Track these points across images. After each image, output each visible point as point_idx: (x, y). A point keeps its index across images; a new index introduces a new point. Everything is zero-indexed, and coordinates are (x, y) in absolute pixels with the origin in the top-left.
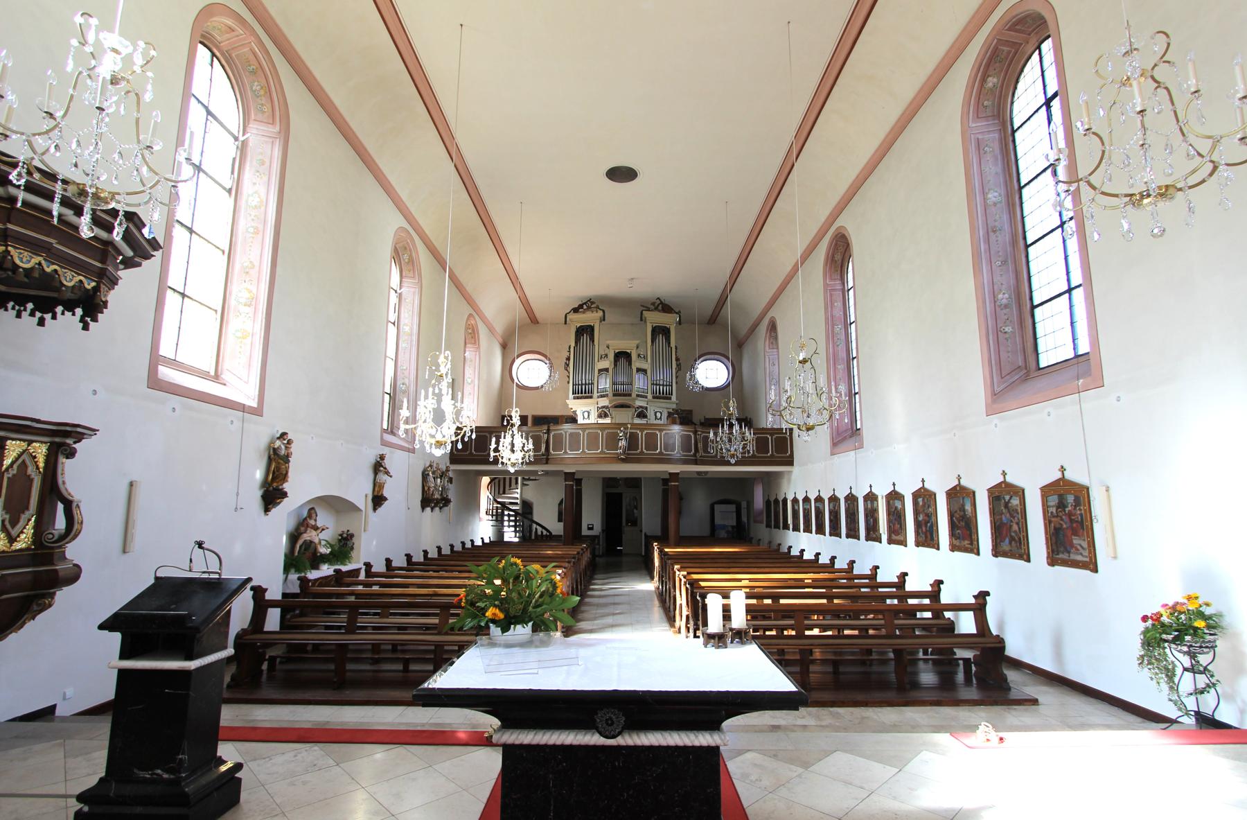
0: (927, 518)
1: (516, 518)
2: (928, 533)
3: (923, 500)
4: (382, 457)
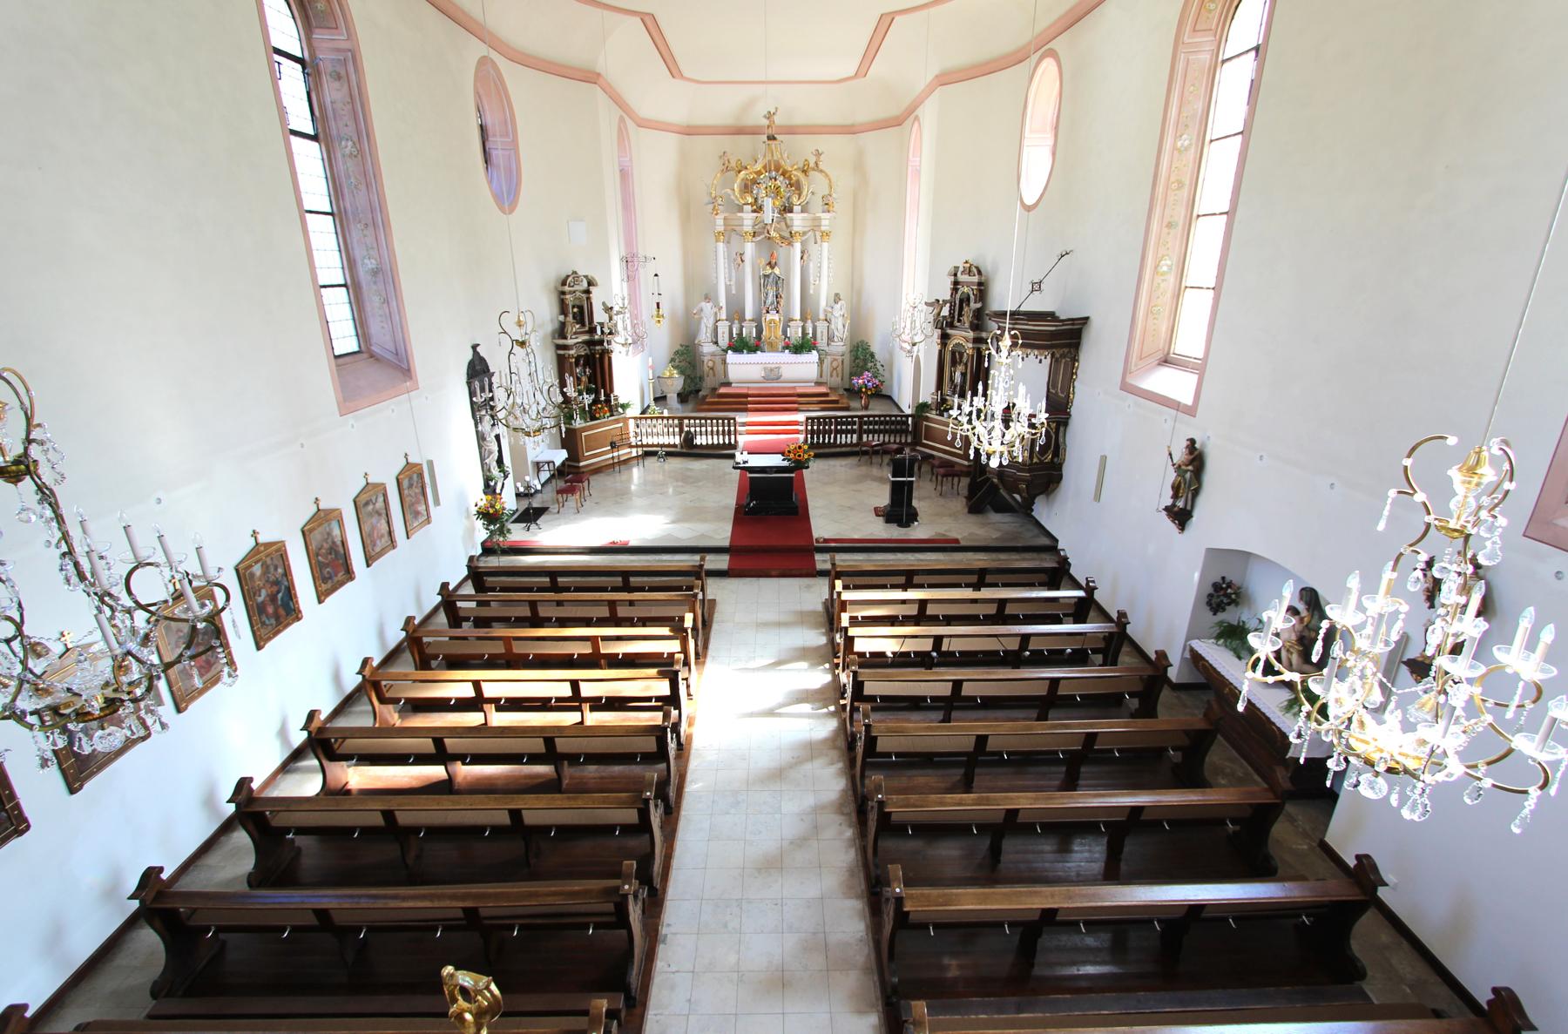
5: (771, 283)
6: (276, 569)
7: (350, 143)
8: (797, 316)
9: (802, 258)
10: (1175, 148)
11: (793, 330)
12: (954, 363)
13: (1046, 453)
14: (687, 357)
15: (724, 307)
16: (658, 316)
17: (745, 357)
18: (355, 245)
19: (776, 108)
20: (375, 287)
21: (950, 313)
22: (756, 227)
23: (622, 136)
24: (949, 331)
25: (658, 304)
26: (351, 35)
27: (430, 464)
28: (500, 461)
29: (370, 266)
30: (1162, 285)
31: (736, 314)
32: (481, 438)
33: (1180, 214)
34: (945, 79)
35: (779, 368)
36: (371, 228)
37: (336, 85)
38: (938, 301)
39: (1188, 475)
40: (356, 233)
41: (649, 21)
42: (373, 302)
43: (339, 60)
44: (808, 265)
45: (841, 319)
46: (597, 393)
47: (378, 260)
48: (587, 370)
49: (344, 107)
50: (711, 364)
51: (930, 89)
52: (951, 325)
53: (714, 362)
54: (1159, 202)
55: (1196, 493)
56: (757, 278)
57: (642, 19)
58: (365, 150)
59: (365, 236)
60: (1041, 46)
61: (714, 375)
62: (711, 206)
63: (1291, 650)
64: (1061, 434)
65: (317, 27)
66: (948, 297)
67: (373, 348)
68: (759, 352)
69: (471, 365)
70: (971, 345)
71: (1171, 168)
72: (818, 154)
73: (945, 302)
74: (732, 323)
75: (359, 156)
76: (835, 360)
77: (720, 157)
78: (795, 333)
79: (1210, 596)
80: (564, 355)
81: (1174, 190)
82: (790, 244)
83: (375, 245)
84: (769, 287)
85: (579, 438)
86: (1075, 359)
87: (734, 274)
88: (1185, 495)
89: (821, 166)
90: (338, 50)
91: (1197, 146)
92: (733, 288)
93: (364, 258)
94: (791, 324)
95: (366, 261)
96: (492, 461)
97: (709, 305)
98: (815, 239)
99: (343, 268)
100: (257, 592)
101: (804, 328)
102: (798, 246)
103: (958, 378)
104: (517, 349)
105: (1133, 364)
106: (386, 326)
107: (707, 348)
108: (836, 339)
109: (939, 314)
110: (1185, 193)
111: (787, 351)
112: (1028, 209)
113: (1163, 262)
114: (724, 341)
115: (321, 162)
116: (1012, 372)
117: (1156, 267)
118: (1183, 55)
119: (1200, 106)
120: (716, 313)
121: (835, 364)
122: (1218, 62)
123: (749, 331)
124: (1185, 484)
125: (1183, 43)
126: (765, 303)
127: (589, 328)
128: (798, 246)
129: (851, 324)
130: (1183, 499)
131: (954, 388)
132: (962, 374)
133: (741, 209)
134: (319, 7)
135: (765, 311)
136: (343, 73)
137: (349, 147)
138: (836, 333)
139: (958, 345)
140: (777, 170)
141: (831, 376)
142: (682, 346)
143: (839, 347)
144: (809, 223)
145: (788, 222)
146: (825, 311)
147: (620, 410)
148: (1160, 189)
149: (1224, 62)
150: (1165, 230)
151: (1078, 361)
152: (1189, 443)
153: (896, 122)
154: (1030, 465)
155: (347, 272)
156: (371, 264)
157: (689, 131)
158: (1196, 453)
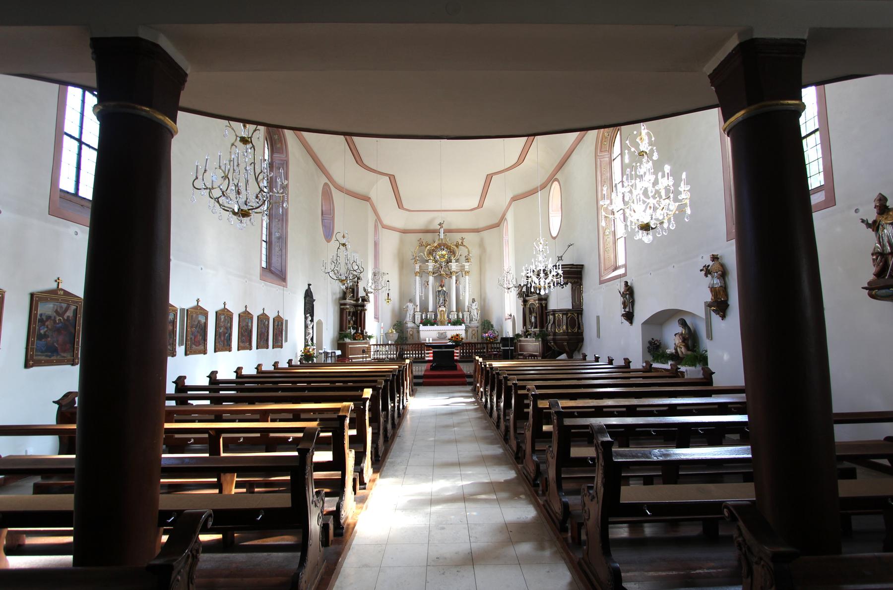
0: (226, 331)
1: (424, 355)
2: (225, 341)
3: (225, 317)
4: (626, 283)
5: (442, 295)
6: (228, 323)
8: (454, 309)
11: (452, 316)
12: (531, 313)
13: (574, 328)
14: (399, 325)
16: (388, 299)
17: (429, 327)
19: (444, 221)
23: (376, 227)
24: (527, 298)
25: (388, 294)
26: (287, 155)
27: (287, 321)
28: (312, 339)
31: (424, 309)
32: (306, 327)
34: (515, 199)
35: (445, 332)
39: (627, 296)
40: (274, 224)
42: (276, 250)
43: (281, 163)
44: (459, 286)
45: (476, 310)
46: (357, 330)
50: (411, 333)
51: (510, 204)
52: (527, 296)
53: (413, 332)
56: (435, 292)
60: (552, 179)
61: (413, 338)
62: (414, 260)
63: (681, 346)
64: (580, 319)
65: (276, 152)
67: (272, 268)
68: (436, 325)
70: (537, 302)
72: (463, 239)
74: (423, 314)
76: (474, 330)
77: (418, 241)
78: (453, 317)
79: (648, 348)
82: (451, 277)
84: (440, 296)
85: (347, 348)
86: (581, 284)
87: (423, 291)
89: (464, 244)
90: (281, 160)
91: (610, 189)
92: (423, 297)
94: (452, 313)
95: (276, 234)
96: (309, 338)
98: (462, 275)
99: (266, 235)
100: (220, 327)
101: (458, 315)
102: (454, 278)
103: (533, 320)
104: (341, 246)
107: (410, 325)
109: (521, 290)
111: (449, 324)
112: (554, 238)
116: (545, 254)
117: (604, 233)
119: (608, 175)
120: (414, 309)
121: (474, 332)
122: (611, 161)
123: (431, 316)
128: (454, 278)
129: (481, 313)
132: (535, 317)
133: (427, 261)
135: (438, 306)
138: (474, 317)
140: (444, 246)
141: (472, 338)
142: (397, 322)
143: (475, 323)
144: (459, 268)
145: (450, 268)
146: (468, 306)
147: (368, 339)
149: (614, 160)
153: (497, 225)
155: (268, 237)
156: (277, 235)
157: (405, 232)
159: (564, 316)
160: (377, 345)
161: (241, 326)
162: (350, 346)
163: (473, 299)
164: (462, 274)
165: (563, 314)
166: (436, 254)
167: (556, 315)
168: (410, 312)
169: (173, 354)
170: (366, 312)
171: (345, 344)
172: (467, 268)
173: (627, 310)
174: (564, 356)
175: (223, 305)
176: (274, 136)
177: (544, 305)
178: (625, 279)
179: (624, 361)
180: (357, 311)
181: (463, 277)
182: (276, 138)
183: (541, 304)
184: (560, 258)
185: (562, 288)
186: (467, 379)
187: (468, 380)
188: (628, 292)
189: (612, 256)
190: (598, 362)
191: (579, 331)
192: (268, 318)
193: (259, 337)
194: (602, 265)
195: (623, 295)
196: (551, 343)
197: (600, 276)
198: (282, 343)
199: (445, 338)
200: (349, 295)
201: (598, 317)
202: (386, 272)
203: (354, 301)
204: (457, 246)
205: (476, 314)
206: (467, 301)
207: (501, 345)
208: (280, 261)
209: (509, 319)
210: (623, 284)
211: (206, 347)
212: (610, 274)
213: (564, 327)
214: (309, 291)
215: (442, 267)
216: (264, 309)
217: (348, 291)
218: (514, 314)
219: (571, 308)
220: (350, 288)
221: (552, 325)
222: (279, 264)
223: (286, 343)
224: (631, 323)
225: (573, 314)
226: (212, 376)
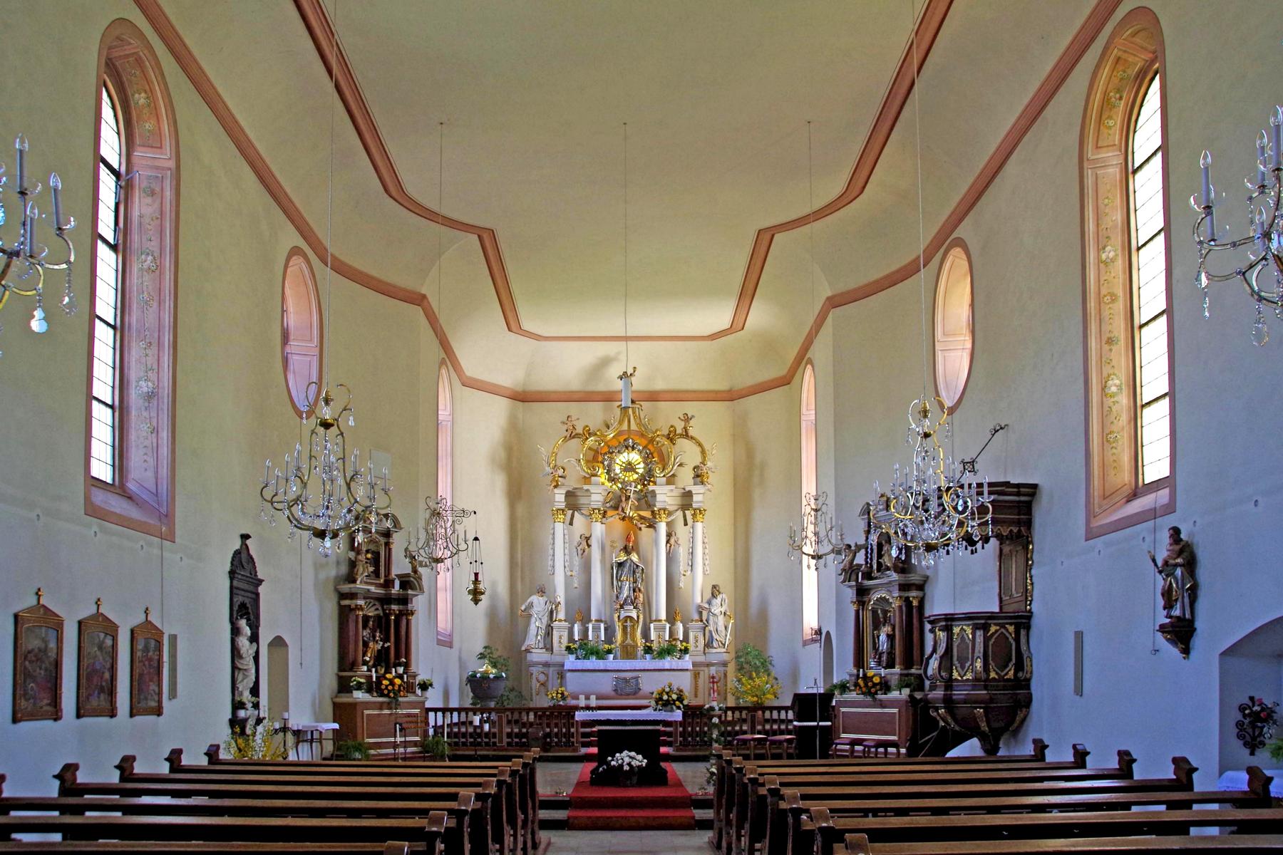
4: (1176, 532)
7: (150, 258)
8: (663, 616)
9: (668, 542)
10: (1099, 261)
12: (877, 626)
13: (1007, 666)
15: (563, 603)
18: (133, 364)
20: (145, 414)
21: (867, 562)
22: (608, 505)
27: (173, 639)
28: (255, 691)
29: (145, 390)
30: (1114, 409)
31: (581, 613)
32: (235, 652)
33: (1119, 328)
34: (834, 302)
36: (154, 348)
37: (149, 200)
38: (849, 546)
39: (1179, 572)
41: (486, 236)
43: (157, 177)
47: (156, 384)
48: (378, 634)
49: (151, 222)
50: (542, 678)
52: (868, 576)
54: (1093, 318)
55: (1193, 592)
56: (608, 566)
57: (479, 236)
58: (165, 266)
59: (147, 355)
60: (944, 241)
64: (1023, 640)
66: (862, 541)
69: (237, 554)
71: (1099, 281)
73: (859, 548)
75: (158, 272)
79: (1239, 725)
80: (350, 606)
81: (1108, 304)
82: (652, 526)
83: (155, 367)
85: (359, 719)
88: (1180, 597)
90: (157, 168)
93: (139, 379)
97: (543, 600)
102: (662, 528)
105: (1096, 506)
106: (148, 459)
108: (715, 644)
110: (1120, 305)
113: (1110, 382)
114: (560, 638)
115: (114, 273)
117: (1103, 389)
118: (1090, 171)
119: (1118, 217)
120: (551, 612)
122: (1129, 171)
123: (596, 635)
124: (1177, 584)
125: (1088, 160)
126: (617, 597)
127: (385, 581)
128: (662, 528)
129: (735, 625)
130: (1178, 605)
131: (880, 658)
132: (888, 636)
134: (147, 127)
136: (158, 189)
137: (149, 262)
138: (715, 636)
139: (883, 600)
148: (1092, 304)
150: (1106, 347)
151: (1032, 542)
152: (1171, 531)
154: (985, 681)
158: (1182, 543)
159: (979, 633)
160: (444, 710)
161: (23, 648)
162: (366, 712)
163: (714, 587)
164: (685, 516)
165: (976, 628)
166: (611, 459)
167: (956, 630)
168: (537, 625)
169: (57, 715)
170: (413, 619)
171: (354, 706)
172: (697, 499)
173: (1177, 612)
174: (971, 748)
175: (96, 607)
176: (137, 96)
177: (915, 603)
178: (1171, 521)
179: (1117, 758)
180: (387, 616)
181: (686, 524)
182: (142, 101)
183: (907, 599)
184: (970, 465)
185: (972, 552)
186: (695, 811)
187: (699, 814)
188: (1179, 560)
189: (1126, 459)
190: (1083, 766)
191: (1020, 674)
192: (111, 629)
193: (84, 681)
194: (1096, 482)
195: (1166, 569)
196: (937, 709)
197: (1090, 515)
198: (160, 702)
199: (635, 693)
200: (364, 571)
201: (1079, 636)
202: (469, 508)
203: (378, 586)
204: (671, 437)
205: (721, 628)
206: (696, 586)
207: (791, 715)
208: (151, 462)
209: (813, 641)
210: (1165, 537)
211: (115, 702)
212: (1119, 508)
213: (979, 664)
214: (244, 556)
215: (628, 498)
216: (146, 612)
217: (362, 557)
218: (831, 627)
219: (997, 609)
220: (367, 551)
221: (941, 657)
222: (150, 474)
223: (174, 701)
224: (1186, 651)
225: (1002, 626)
226: (66, 775)
